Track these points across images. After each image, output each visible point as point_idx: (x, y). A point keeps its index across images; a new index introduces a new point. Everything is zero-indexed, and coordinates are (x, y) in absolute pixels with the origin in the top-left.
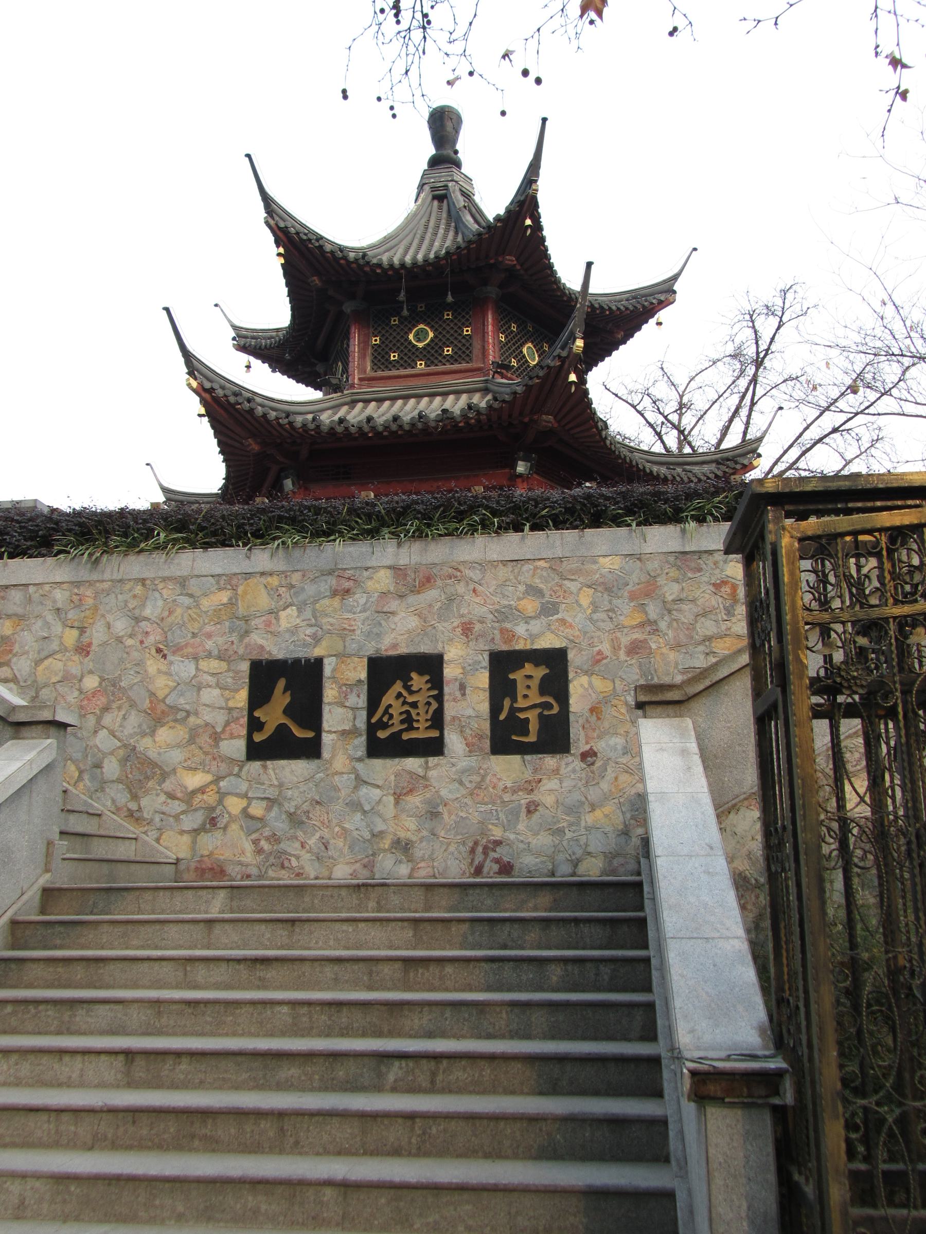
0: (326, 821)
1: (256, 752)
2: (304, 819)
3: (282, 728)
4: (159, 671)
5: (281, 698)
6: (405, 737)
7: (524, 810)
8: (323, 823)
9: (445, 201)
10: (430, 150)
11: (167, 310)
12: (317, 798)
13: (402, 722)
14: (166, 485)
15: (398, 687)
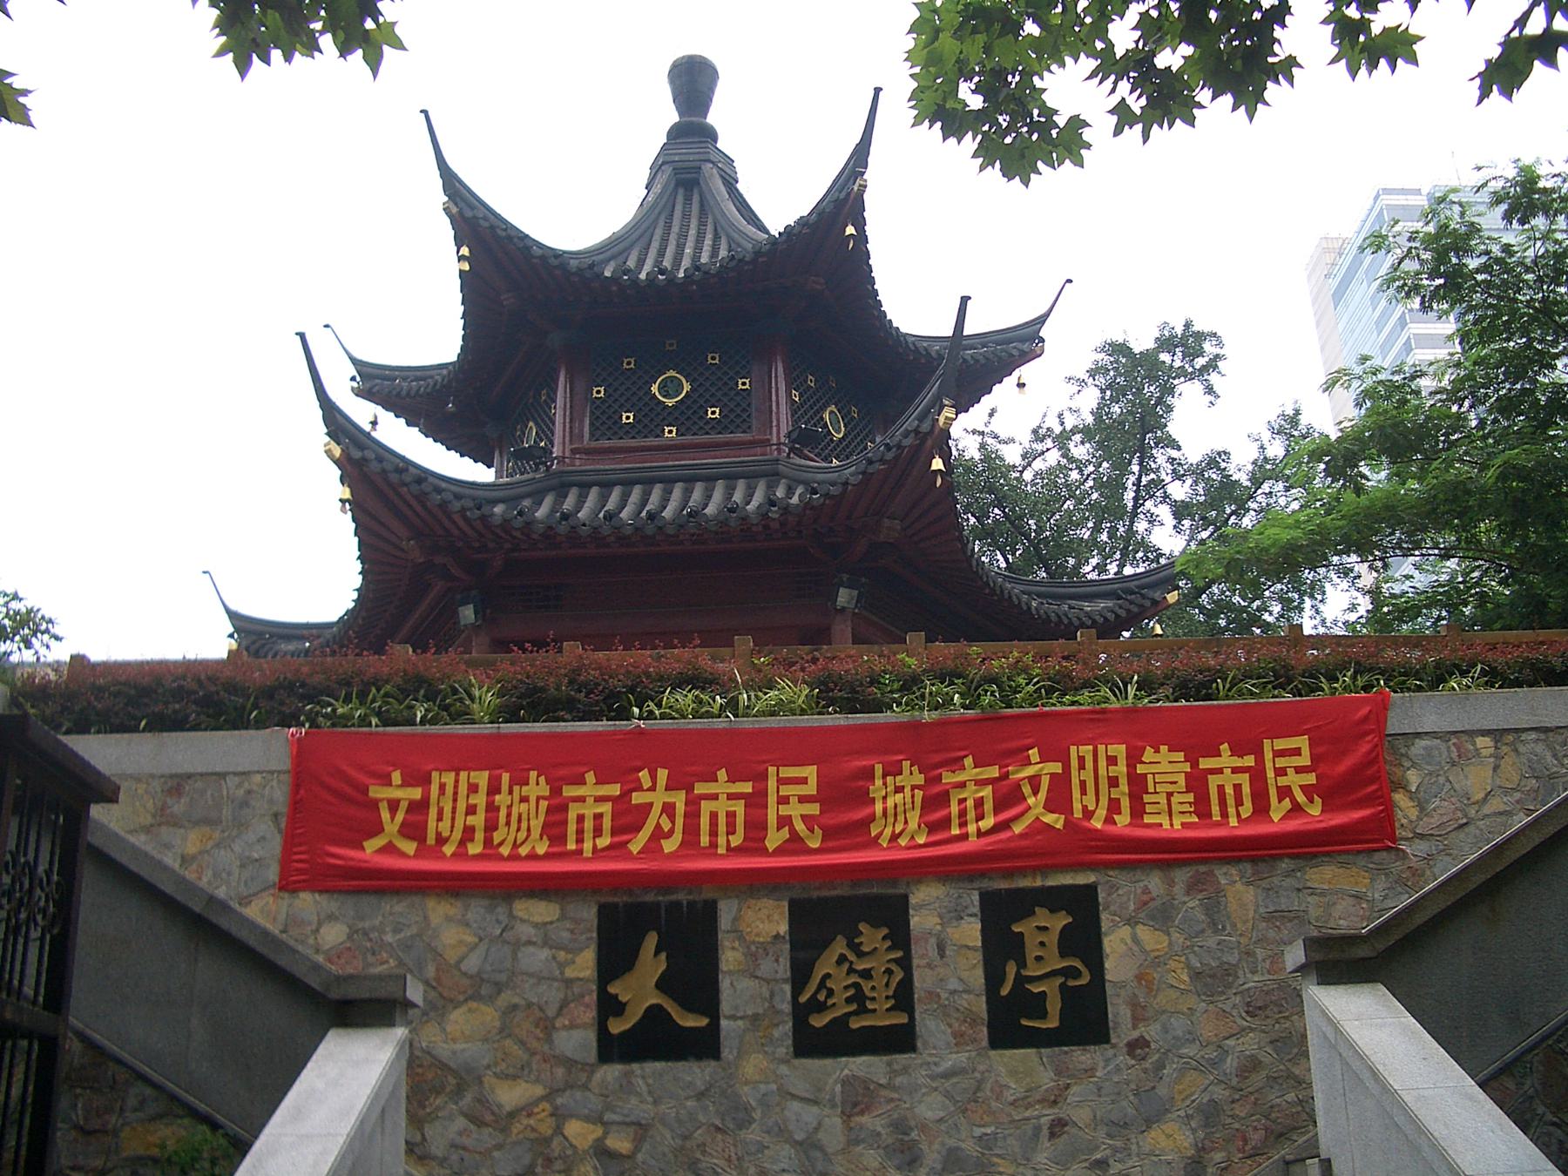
0: (734, 1157)
1: (611, 1049)
2: (698, 1155)
3: (655, 1013)
4: (449, 919)
5: (651, 964)
6: (855, 1024)
7: (1045, 1132)
8: (729, 1160)
9: (696, 191)
10: (670, 116)
11: (302, 336)
12: (718, 1122)
13: (848, 1001)
14: (233, 607)
15: (839, 947)
